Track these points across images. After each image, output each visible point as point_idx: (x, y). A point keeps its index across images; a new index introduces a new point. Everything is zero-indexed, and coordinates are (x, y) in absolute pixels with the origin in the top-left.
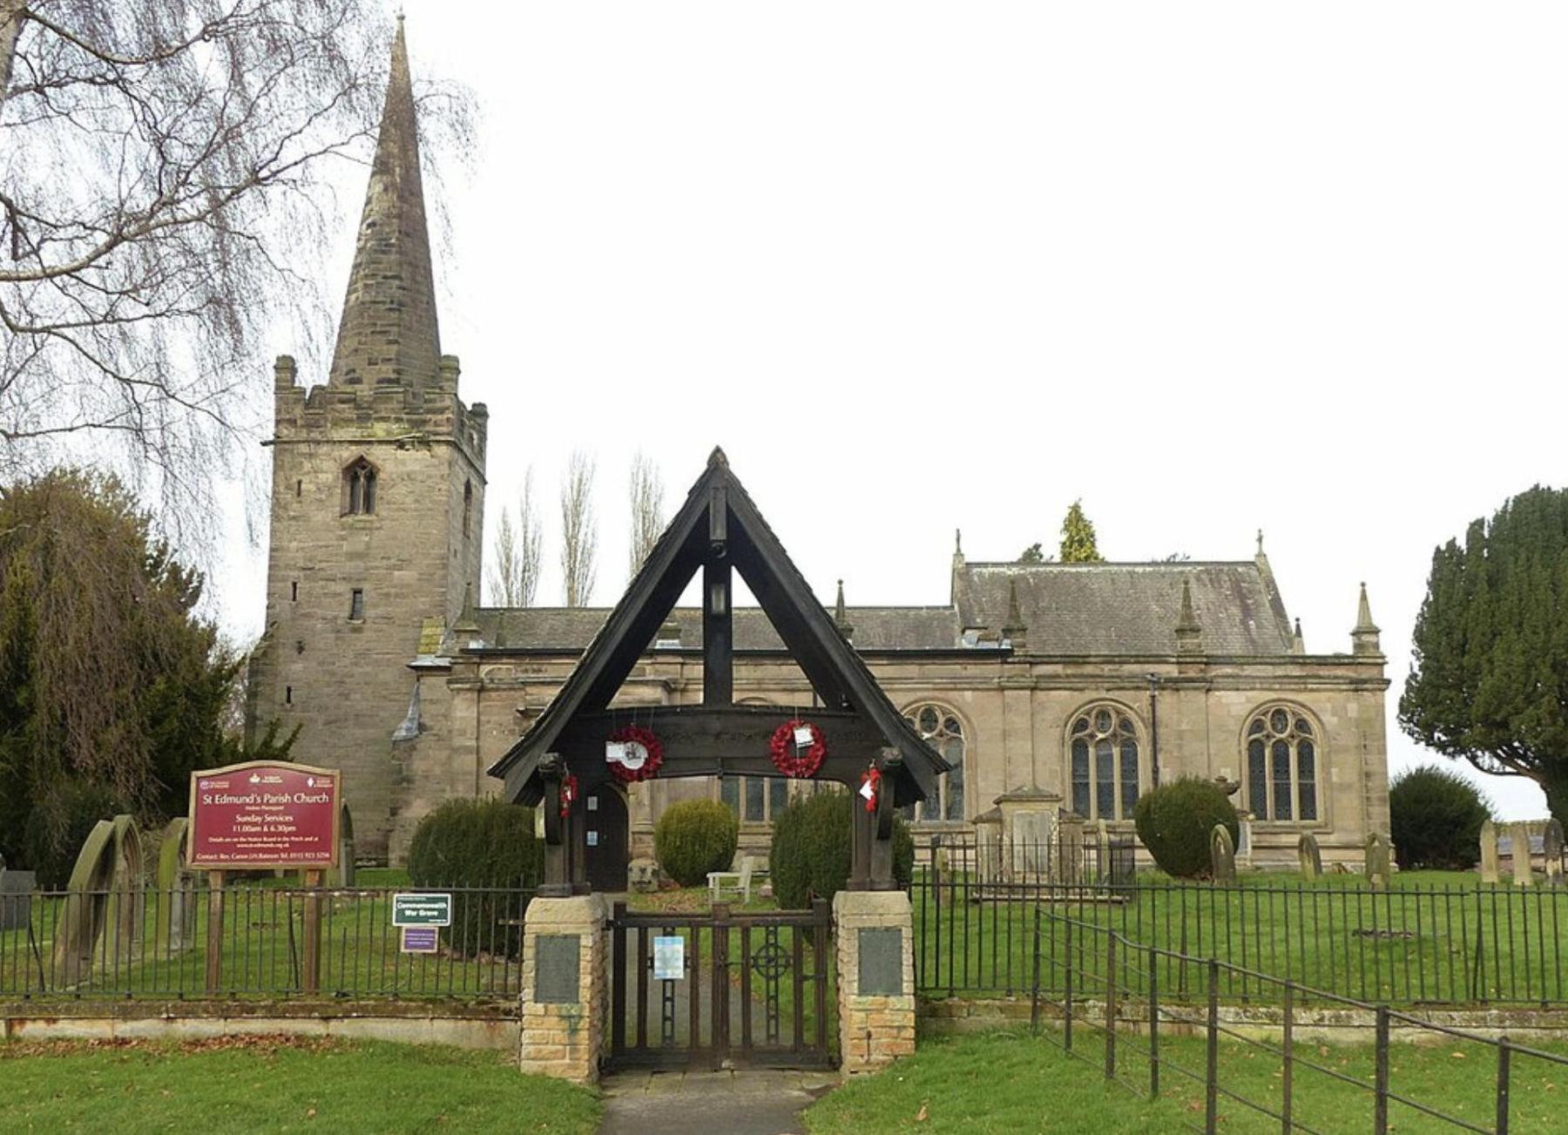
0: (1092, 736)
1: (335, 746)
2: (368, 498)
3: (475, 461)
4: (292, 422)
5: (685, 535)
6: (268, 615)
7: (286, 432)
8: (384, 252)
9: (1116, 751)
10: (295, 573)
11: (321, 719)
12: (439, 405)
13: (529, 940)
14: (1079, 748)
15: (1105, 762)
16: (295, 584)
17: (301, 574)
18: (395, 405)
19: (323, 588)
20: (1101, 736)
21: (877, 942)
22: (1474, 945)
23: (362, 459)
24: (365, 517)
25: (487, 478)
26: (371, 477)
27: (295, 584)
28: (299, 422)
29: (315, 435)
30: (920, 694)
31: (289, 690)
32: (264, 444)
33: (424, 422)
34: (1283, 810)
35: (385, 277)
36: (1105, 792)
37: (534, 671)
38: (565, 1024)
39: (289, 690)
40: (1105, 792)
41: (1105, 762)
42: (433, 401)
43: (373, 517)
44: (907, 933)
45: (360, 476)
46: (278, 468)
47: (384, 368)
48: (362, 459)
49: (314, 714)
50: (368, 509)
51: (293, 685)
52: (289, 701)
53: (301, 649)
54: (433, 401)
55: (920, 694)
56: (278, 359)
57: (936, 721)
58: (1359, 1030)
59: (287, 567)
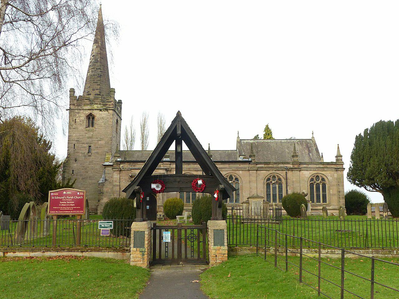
0: (271, 182)
4: (74, 105)
7: (72, 107)
8: (96, 63)
9: (277, 186)
12: (110, 100)
13: (132, 232)
14: (268, 185)
15: (274, 188)
16: (74, 145)
17: (76, 142)
18: (99, 100)
19: (81, 145)
20: (273, 182)
21: (218, 233)
22: (366, 234)
23: (91, 114)
26: (93, 118)
27: (74, 145)
30: (229, 172)
31: (73, 171)
32: (67, 110)
33: (106, 105)
34: (318, 200)
35: (97, 69)
36: (274, 196)
38: (141, 253)
39: (73, 171)
40: (274, 196)
41: (274, 188)
44: (225, 231)
47: (96, 91)
48: (91, 114)
50: (93, 126)
51: (74, 170)
53: (76, 161)
55: (229, 172)
58: (337, 255)
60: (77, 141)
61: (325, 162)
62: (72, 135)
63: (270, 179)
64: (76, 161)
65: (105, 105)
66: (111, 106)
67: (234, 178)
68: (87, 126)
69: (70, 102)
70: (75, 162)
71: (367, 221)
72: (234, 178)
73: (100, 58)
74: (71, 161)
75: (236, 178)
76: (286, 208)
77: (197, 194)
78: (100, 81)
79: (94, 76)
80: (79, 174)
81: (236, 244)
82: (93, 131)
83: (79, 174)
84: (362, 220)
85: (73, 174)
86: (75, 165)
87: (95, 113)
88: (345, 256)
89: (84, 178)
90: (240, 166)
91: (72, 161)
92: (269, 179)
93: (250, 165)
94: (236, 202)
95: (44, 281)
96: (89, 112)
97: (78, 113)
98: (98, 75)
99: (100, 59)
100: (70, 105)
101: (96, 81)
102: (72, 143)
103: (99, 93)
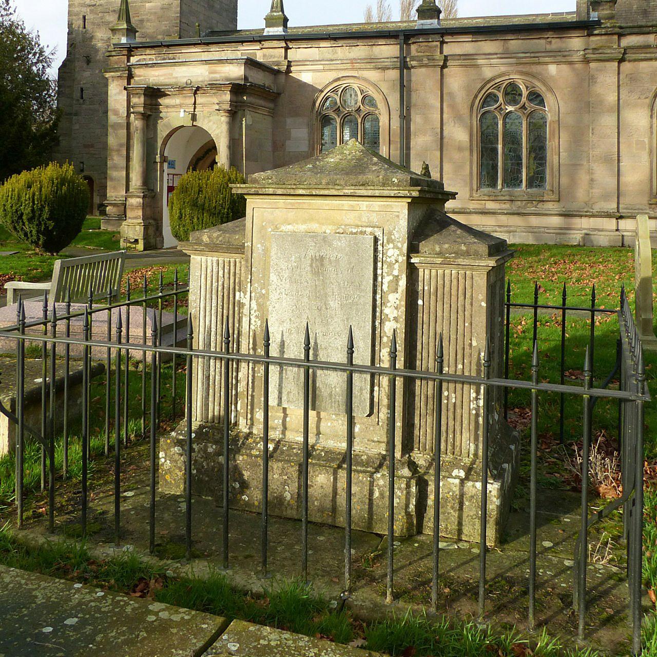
16: (84, 17)
27: (84, 17)
31: (82, 90)
53: (88, 62)
57: (521, 95)
60: (90, 6)
61: (458, 17)
63: (495, 96)
64: (88, 62)
67: (525, 93)
70: (85, 65)
71: (564, 310)
72: (525, 93)
74: (77, 64)
75: (531, 94)
77: (374, 158)
81: (356, 376)
84: (539, 303)
85: (81, 101)
86: (87, 74)
88: (122, 509)
90: (548, 47)
91: (79, 64)
92: (490, 98)
93: (592, 38)
94: (530, 184)
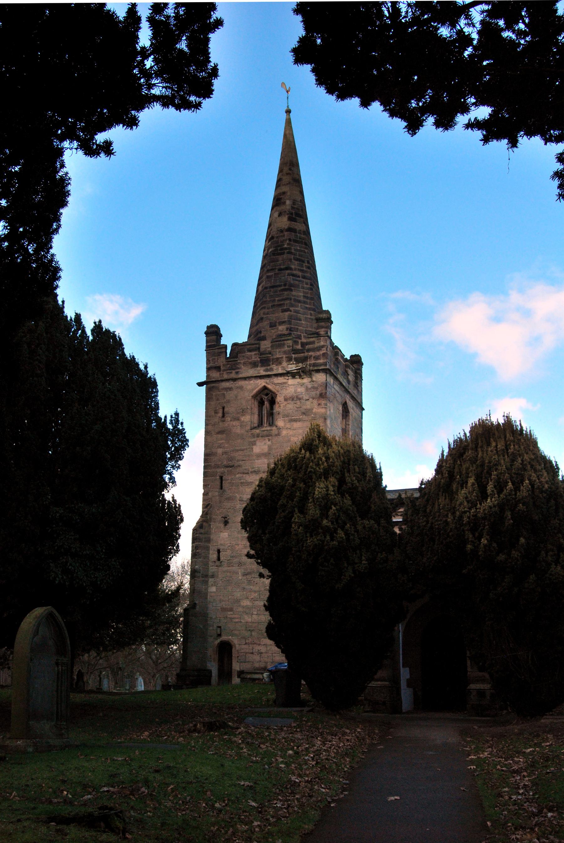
1: (251, 591)
2: (271, 414)
3: (351, 388)
4: (218, 368)
5: (477, 718)
6: (204, 500)
7: (215, 375)
10: (219, 470)
11: (240, 571)
12: (316, 345)
16: (221, 478)
17: (226, 470)
18: (286, 348)
23: (265, 388)
24: (269, 428)
25: (364, 406)
26: (273, 402)
27: (221, 478)
28: (222, 368)
29: (233, 375)
31: (219, 551)
32: (200, 384)
35: (280, 270)
37: (171, 420)
39: (219, 551)
42: (313, 343)
43: (274, 428)
45: (266, 400)
46: (208, 399)
48: (265, 388)
49: (235, 568)
50: (272, 424)
51: (221, 548)
52: (219, 559)
53: (226, 523)
54: (313, 343)
56: (208, 327)
59: (217, 466)
62: (214, 450)
65: (304, 360)
66: (321, 361)
68: (256, 425)
69: (208, 361)
70: (222, 525)
73: (287, 241)
76: (183, 650)
78: (291, 299)
79: (272, 290)
80: (236, 560)
82: (269, 435)
83: (236, 560)
87: (272, 384)
89: (249, 570)
95: (200, 817)
96: (261, 383)
97: (230, 389)
98: (285, 285)
99: (288, 244)
100: (208, 369)
101: (279, 301)
102: (214, 475)
103: (286, 332)
